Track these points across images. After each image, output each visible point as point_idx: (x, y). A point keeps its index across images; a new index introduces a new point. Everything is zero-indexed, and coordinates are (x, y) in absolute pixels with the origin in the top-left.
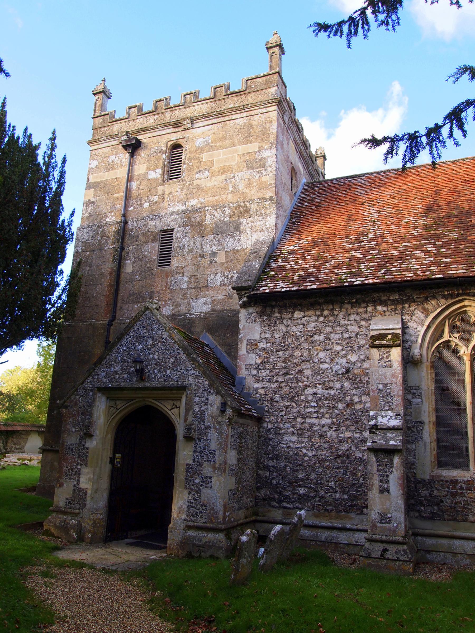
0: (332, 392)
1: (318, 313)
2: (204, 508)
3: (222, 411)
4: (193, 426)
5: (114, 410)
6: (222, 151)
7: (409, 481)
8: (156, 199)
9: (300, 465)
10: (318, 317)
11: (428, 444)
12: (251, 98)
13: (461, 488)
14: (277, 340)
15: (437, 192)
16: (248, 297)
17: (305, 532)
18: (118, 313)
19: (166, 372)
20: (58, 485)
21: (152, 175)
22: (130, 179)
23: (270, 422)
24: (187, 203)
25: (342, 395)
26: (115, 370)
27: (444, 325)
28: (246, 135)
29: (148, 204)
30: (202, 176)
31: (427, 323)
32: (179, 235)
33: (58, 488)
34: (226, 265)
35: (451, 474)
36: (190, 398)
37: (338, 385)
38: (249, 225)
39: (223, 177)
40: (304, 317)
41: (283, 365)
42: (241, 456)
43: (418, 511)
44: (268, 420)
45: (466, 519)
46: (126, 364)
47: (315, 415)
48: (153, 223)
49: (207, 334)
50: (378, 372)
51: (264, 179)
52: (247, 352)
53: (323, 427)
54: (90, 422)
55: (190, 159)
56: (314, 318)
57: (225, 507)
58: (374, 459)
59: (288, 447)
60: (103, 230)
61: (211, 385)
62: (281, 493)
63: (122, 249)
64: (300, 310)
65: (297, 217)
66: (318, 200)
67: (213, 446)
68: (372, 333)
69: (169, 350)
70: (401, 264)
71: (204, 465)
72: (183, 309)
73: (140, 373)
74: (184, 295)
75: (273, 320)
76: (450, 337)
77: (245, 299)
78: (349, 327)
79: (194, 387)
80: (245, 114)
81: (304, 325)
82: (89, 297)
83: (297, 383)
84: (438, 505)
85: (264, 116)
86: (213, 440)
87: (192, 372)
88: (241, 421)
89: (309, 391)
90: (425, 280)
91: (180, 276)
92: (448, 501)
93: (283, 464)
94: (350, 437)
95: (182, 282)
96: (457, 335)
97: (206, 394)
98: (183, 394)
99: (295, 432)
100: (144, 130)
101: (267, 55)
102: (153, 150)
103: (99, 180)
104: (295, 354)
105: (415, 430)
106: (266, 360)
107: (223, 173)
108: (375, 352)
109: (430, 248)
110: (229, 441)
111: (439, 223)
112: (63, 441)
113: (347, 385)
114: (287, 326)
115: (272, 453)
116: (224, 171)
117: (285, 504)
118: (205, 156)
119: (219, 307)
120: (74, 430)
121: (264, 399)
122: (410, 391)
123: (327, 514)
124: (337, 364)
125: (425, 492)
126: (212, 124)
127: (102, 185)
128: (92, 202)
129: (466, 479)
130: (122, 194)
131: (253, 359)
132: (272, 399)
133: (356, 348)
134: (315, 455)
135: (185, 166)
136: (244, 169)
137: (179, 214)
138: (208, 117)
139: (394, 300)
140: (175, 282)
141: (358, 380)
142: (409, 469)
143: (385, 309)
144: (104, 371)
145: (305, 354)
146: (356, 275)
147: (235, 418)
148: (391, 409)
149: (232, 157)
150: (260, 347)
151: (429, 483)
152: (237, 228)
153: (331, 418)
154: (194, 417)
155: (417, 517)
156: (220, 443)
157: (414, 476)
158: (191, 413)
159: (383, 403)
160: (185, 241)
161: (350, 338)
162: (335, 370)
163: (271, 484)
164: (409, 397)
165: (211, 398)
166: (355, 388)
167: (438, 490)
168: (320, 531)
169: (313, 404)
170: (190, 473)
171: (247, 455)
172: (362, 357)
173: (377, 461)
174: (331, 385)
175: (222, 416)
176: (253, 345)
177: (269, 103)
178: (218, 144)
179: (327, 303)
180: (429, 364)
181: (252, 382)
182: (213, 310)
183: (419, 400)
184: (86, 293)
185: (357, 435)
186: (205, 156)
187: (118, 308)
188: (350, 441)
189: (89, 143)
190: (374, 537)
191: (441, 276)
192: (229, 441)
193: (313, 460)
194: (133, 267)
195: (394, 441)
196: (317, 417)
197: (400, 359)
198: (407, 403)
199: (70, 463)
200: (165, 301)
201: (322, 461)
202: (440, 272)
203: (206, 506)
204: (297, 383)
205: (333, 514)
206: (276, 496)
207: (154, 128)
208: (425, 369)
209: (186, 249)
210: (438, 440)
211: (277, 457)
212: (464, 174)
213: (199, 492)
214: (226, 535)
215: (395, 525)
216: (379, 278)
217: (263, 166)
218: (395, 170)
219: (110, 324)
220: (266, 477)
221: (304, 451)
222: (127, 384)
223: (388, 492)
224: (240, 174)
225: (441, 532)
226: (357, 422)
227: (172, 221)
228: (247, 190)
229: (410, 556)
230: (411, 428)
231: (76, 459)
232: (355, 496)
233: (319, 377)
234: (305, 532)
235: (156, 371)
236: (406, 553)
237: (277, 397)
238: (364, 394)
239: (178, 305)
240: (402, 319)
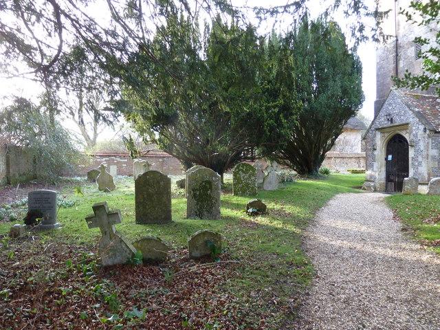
48: (410, 36)
63: (397, 55)
67: (422, 148)
73: (392, 121)
165: (420, 126)
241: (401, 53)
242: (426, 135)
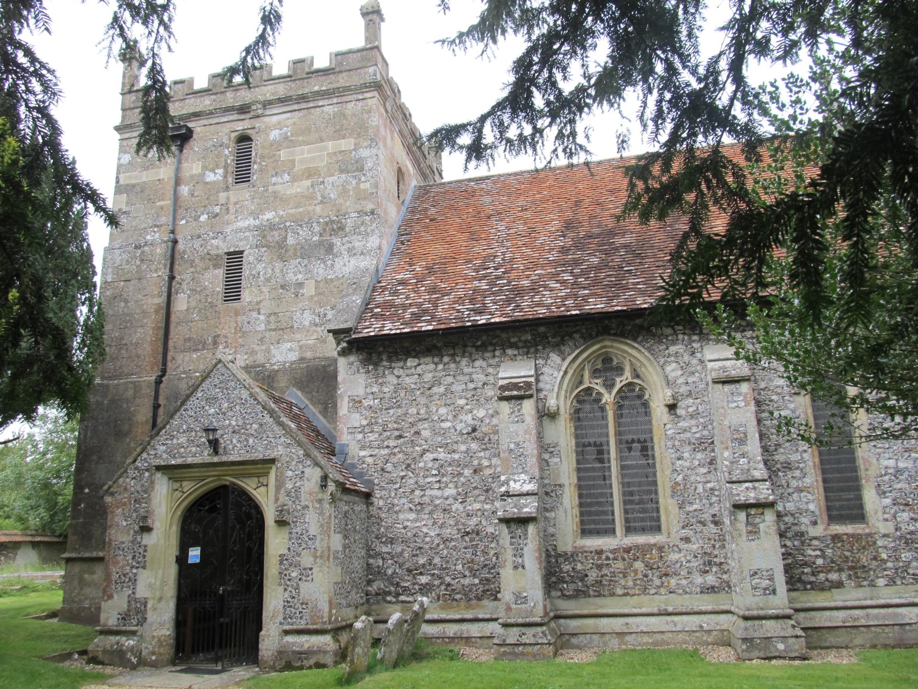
0: (456, 456)
1: (436, 359)
2: (304, 606)
3: (322, 486)
4: (286, 507)
5: (180, 494)
6: (306, 148)
7: (548, 556)
8: (217, 209)
9: (420, 548)
10: (436, 364)
11: (569, 510)
12: (342, 81)
13: (608, 558)
14: (387, 395)
15: (577, 203)
16: (349, 342)
17: (427, 629)
18: (169, 364)
19: (247, 440)
20: (106, 598)
21: (210, 177)
22: (178, 182)
23: (381, 498)
24: (260, 217)
25: (468, 458)
26: (181, 443)
27: (583, 369)
28: (338, 127)
29: (206, 216)
30: (279, 180)
31: (564, 369)
32: (251, 259)
33: (106, 601)
34: (316, 299)
35: (596, 544)
36: (281, 473)
37: (463, 448)
38: (345, 247)
39: (308, 183)
40: (419, 365)
41: (396, 426)
42: (347, 541)
43: (560, 590)
44: (378, 496)
45: (614, 593)
46: (194, 433)
47: (437, 486)
49: (294, 389)
50: (509, 428)
51: (362, 186)
52: (349, 412)
53: (447, 499)
54: (147, 511)
55: (263, 157)
56: (432, 366)
57: (330, 602)
58: (507, 531)
59: (405, 528)
60: (143, 252)
61: (307, 455)
62: (398, 584)
63: (172, 278)
64: (414, 357)
65: (407, 234)
66: (433, 211)
67: (313, 530)
68: (501, 383)
69: (250, 413)
70: (533, 297)
71: (303, 553)
72: (260, 358)
73: (214, 445)
74: (261, 340)
75: (381, 369)
76: (590, 383)
77: (345, 345)
78: (474, 376)
79: (285, 459)
80: (335, 100)
81: (419, 375)
82: (125, 344)
83: (413, 447)
84: (582, 580)
85: (360, 104)
86: (312, 522)
87: (283, 439)
88: (345, 498)
89: (429, 456)
90: (559, 317)
91: (255, 314)
92: (593, 575)
93: (399, 549)
94: (480, 509)
95: (258, 322)
96: (598, 381)
97: (301, 467)
98: (271, 468)
99: (413, 508)
100: (197, 115)
101: (361, 22)
102: (211, 143)
103: (134, 182)
104: (410, 411)
105: (553, 494)
106: (373, 421)
107: (308, 178)
108: (504, 405)
109: (567, 277)
110: (333, 523)
111: (579, 245)
112: (110, 540)
113: (474, 446)
114: (399, 377)
115: (386, 536)
116: (310, 173)
117: (402, 598)
118: (283, 154)
119: (309, 355)
120: (125, 523)
121: (373, 470)
122: (545, 448)
123: (455, 603)
124: (461, 421)
125: (567, 567)
126: (292, 111)
127: (138, 189)
128: (125, 213)
129: (612, 548)
130: (168, 203)
131: (357, 420)
132: (383, 469)
133: (482, 400)
134: (439, 535)
135: (256, 167)
136: (336, 173)
137: (250, 230)
138: (286, 101)
139: (525, 341)
140: (249, 323)
141: (486, 439)
142: (547, 538)
143: (516, 352)
144: (163, 444)
145: (422, 411)
146: (480, 312)
147: (339, 495)
148: (524, 471)
149: (320, 156)
150: (366, 405)
151: (572, 556)
152: (330, 248)
153: (456, 487)
154: (287, 496)
155: (559, 597)
156: (322, 526)
157: (555, 550)
158: (282, 491)
159: (515, 465)
160: (260, 267)
161: (475, 389)
162: (458, 428)
163: (386, 575)
164: (546, 456)
165: (308, 471)
166: (484, 449)
167: (582, 563)
168: (447, 625)
169: (434, 472)
170: (284, 565)
171: (355, 541)
172: (490, 412)
173: (509, 533)
174: (455, 447)
175: (323, 492)
176: (356, 403)
177: (366, 87)
178: (301, 138)
179: (446, 345)
180: (567, 416)
181: (357, 450)
182: (302, 359)
183: (558, 460)
184: (122, 339)
185: (487, 507)
186: (283, 154)
187: (169, 358)
188: (479, 513)
189: (117, 129)
190: (509, 621)
191: (577, 312)
192: (333, 523)
193: (436, 542)
194: (188, 302)
195: (529, 507)
196: (440, 488)
197: (533, 412)
198: (544, 464)
199: (122, 567)
200: (236, 347)
201: (445, 541)
202: (577, 307)
203: (307, 604)
204: (413, 447)
205: (463, 603)
206: (393, 589)
207: (212, 113)
208: (563, 422)
209: (262, 278)
210: (581, 505)
211: (392, 541)
212: (611, 181)
213: (297, 588)
214: (333, 637)
215: (532, 604)
216: (507, 315)
217: (361, 169)
218: (528, 172)
219: (159, 382)
220: (378, 567)
221: (425, 530)
222: (198, 460)
223: (523, 567)
224: (331, 179)
225: (586, 612)
226: (487, 491)
227: (241, 240)
228: (341, 201)
229: (549, 637)
230: (547, 493)
231: (130, 561)
232: (487, 580)
233: (440, 439)
234: (427, 629)
235: (234, 441)
236: (545, 635)
237: (389, 467)
238: (494, 456)
239: (253, 353)
240: (536, 365)
241: (184, 275)
242: (327, 497)
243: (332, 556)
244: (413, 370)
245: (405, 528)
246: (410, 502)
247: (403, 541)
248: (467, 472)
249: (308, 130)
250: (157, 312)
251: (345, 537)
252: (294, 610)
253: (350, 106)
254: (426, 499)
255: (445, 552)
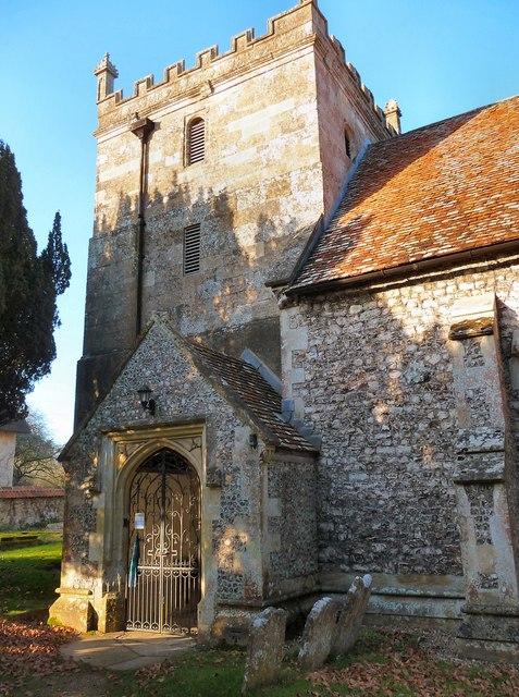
0: (409, 409)
53: (400, 457)
59: (356, 489)
73: (151, 406)
77: (284, 297)
81: (363, 322)
91: (212, 282)
93: (351, 513)
100: (156, 107)
104: (355, 363)
113: (428, 397)
118: (231, 127)
128: (105, 206)
131: (302, 375)
132: (330, 426)
145: (369, 361)
162: (409, 378)
165: (237, 430)
168: (408, 601)
176: (300, 357)
177: (302, 44)
193: (391, 504)
201: (402, 505)
206: (346, 557)
211: (342, 504)
221: (379, 493)
223: (489, 541)
226: (446, 447)
237: (336, 423)
241: (153, 252)
242: (257, 458)
243: (266, 523)
244: (356, 318)
245: (356, 489)
246: (360, 461)
247: (354, 504)
248: (422, 426)
249: (252, 99)
250: (132, 289)
251: (286, 501)
252: (228, 583)
253: (289, 66)
254: (378, 458)
255: (401, 517)
